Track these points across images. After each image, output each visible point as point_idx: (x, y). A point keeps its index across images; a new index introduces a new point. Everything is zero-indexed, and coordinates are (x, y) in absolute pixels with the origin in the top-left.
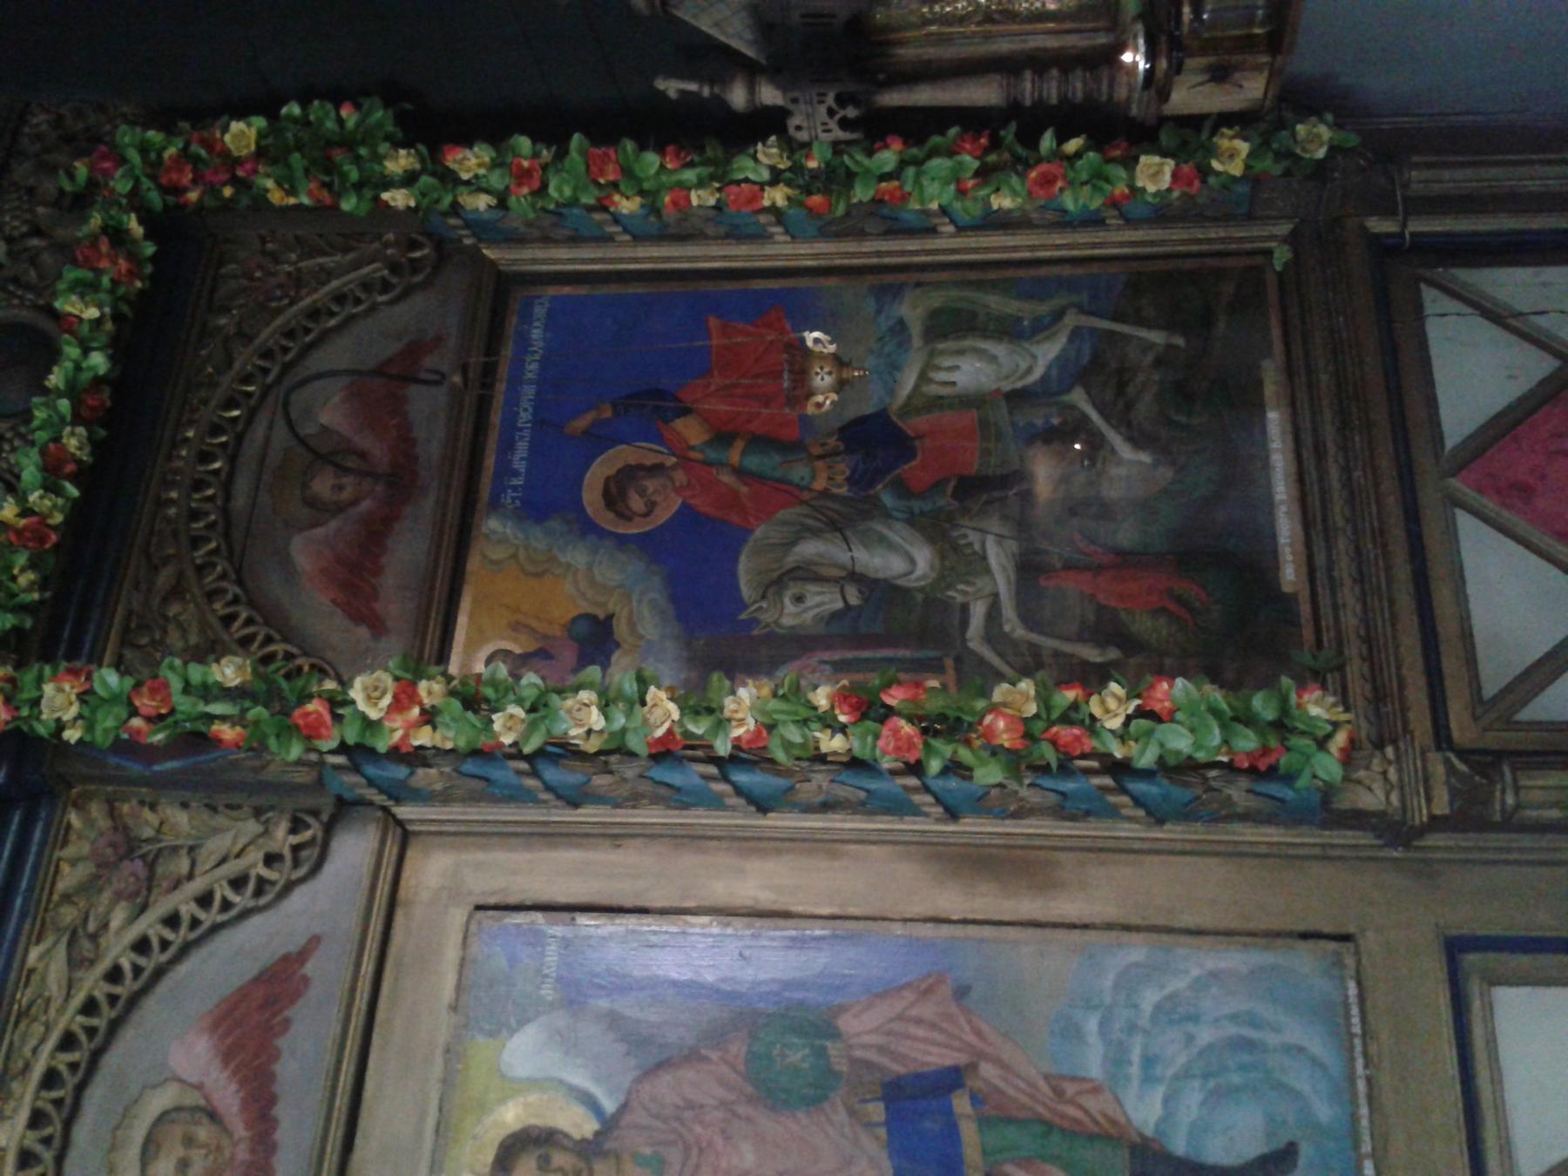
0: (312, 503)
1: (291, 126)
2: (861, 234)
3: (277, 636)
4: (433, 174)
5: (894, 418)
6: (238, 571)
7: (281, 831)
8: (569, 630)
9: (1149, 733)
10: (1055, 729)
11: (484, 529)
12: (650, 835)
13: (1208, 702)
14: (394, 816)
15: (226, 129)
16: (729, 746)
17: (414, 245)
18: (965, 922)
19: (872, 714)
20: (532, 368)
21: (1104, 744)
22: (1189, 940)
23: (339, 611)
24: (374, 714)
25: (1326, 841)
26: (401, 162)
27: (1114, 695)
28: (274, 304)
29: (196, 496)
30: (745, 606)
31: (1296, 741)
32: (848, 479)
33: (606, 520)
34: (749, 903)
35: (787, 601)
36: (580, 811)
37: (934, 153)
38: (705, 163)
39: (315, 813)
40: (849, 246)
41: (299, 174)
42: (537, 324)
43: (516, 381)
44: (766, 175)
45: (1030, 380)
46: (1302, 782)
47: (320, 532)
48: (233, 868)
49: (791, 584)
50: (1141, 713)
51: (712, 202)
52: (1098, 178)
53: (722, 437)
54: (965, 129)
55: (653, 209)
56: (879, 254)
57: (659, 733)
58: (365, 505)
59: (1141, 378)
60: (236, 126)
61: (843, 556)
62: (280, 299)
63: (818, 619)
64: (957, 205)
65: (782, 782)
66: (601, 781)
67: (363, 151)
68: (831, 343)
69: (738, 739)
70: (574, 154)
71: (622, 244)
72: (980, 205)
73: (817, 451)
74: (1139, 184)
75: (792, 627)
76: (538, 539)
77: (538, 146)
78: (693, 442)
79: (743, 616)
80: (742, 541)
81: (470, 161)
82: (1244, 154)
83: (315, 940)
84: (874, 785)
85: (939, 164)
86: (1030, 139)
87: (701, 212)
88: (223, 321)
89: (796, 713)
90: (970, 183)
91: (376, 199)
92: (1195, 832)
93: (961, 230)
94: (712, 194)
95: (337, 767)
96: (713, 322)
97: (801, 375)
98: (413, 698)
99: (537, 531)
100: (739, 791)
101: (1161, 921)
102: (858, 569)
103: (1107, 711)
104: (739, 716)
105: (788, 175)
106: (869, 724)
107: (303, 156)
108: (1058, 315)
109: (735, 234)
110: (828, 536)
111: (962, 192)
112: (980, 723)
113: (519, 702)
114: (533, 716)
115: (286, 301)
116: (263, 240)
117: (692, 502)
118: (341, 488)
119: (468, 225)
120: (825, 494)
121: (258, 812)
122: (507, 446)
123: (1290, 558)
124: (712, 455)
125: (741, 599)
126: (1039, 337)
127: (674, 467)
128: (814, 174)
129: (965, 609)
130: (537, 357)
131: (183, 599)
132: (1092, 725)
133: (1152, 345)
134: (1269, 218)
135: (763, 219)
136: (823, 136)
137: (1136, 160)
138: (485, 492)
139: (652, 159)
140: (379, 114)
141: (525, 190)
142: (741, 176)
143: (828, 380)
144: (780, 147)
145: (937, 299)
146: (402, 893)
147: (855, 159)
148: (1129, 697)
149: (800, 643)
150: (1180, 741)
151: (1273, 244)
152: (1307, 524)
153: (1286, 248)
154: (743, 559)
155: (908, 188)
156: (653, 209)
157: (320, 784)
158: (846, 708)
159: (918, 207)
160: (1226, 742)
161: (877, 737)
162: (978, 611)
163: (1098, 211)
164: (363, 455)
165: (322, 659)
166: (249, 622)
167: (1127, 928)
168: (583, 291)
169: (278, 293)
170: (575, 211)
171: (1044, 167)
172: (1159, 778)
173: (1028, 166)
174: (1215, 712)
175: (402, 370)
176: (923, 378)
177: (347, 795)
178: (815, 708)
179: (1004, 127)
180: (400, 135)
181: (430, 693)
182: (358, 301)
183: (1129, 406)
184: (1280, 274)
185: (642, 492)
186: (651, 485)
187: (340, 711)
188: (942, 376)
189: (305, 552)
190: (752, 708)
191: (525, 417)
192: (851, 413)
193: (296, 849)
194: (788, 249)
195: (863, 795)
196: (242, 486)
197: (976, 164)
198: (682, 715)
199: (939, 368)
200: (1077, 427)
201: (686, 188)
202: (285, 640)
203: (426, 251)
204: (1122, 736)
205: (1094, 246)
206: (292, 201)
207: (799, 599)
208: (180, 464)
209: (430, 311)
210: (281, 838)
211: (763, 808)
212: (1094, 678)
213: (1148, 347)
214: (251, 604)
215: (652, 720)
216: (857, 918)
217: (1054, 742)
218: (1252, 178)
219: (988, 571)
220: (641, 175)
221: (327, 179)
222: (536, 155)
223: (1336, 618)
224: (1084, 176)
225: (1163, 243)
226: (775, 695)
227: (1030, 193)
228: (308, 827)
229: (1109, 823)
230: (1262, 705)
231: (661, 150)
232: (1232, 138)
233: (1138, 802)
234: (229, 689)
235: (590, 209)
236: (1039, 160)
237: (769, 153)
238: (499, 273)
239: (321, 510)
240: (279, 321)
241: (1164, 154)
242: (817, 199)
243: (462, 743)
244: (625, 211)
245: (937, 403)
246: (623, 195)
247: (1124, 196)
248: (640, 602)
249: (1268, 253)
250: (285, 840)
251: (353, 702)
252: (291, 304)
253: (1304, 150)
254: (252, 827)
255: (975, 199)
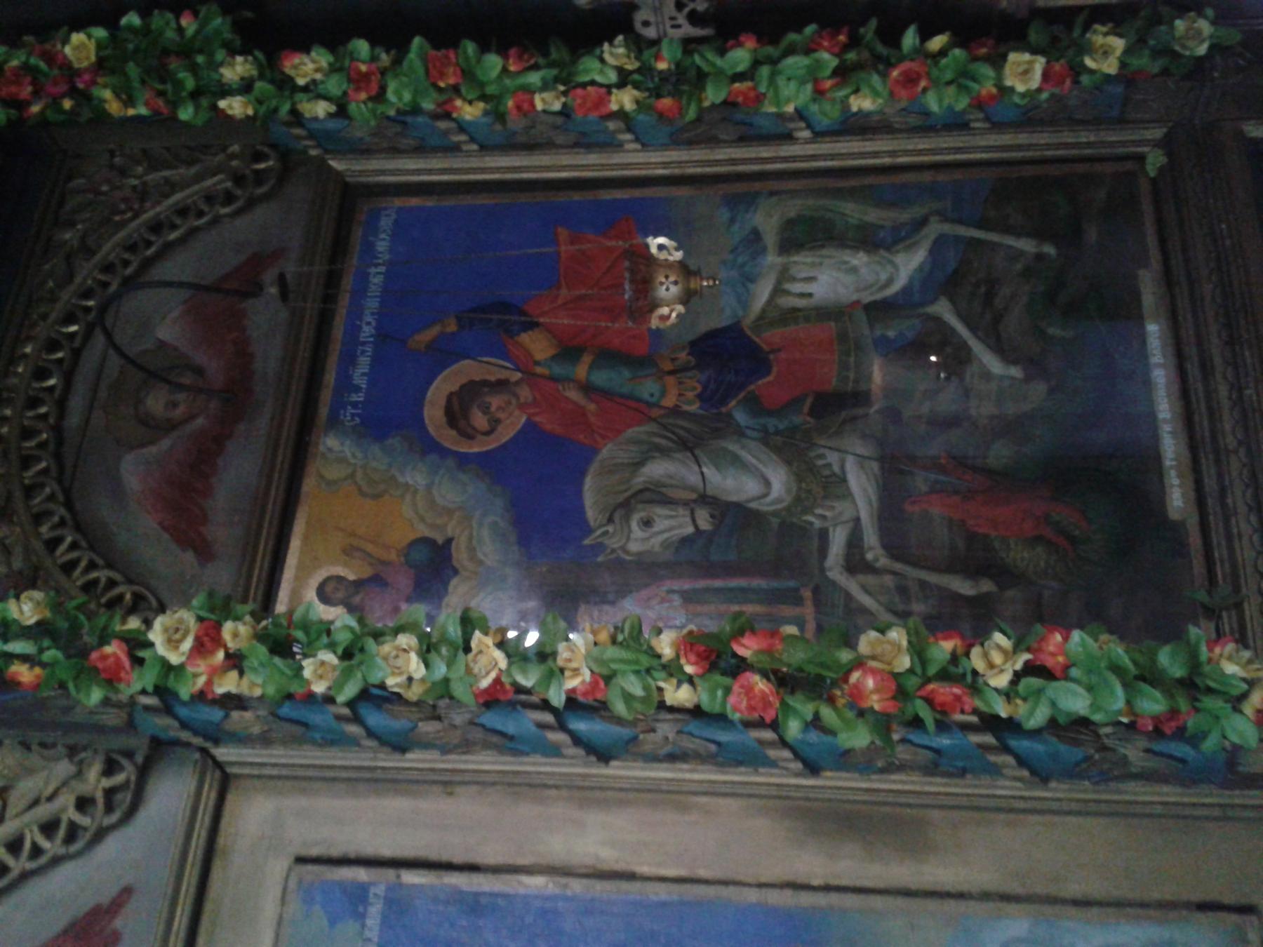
0: (146, 421)
1: (131, 37)
2: (712, 141)
3: (100, 562)
4: (272, 82)
5: (749, 333)
6: (67, 492)
7: (93, 773)
8: (406, 556)
9: (1039, 692)
10: (931, 686)
11: (322, 448)
12: (481, 782)
13: (1109, 658)
14: (213, 758)
15: (66, 41)
16: (563, 698)
17: (259, 157)
18: (827, 888)
19: (722, 664)
20: (376, 280)
21: (987, 703)
22: (1073, 911)
23: (166, 536)
24: (175, 659)
25: (1227, 801)
26: (236, 69)
27: (999, 647)
28: (117, 218)
29: (30, 414)
30: (590, 531)
31: (1208, 702)
32: (699, 396)
33: (448, 438)
34: (589, 861)
35: (634, 525)
36: (409, 756)
37: (791, 51)
38: (551, 65)
39: (129, 755)
40: (698, 154)
41: (136, 84)
42: (383, 236)
43: (360, 292)
44: (613, 77)
45: (889, 292)
46: (1209, 745)
47: (153, 449)
48: (44, 812)
49: (640, 506)
50: (1030, 669)
51: (557, 106)
52: (963, 77)
53: (569, 351)
54: (823, 26)
55: (499, 116)
56: (733, 162)
57: (485, 683)
58: (200, 421)
59: (1005, 291)
60: (77, 38)
61: (693, 479)
62: (123, 212)
63: (666, 545)
64: (814, 108)
65: (626, 732)
66: (428, 728)
67: (200, 59)
68: (677, 249)
69: (573, 690)
70: (413, 55)
71: (469, 154)
72: (838, 107)
73: (668, 366)
74: (1008, 83)
75: (639, 554)
76: (377, 458)
77: (378, 50)
78: (539, 356)
79: (587, 542)
80: (588, 460)
81: (307, 66)
82: (1118, 52)
83: (127, 892)
84: (724, 737)
85: (796, 63)
86: (891, 37)
87: (550, 119)
88: (68, 236)
89: (637, 662)
90: (828, 84)
91: (214, 107)
92: (1085, 791)
93: (819, 135)
94: (558, 98)
95: (147, 708)
96: (563, 233)
97: (644, 285)
98: (218, 642)
99: (376, 449)
100: (577, 740)
101: (1040, 889)
102: (709, 492)
103: (991, 666)
104: (574, 665)
105: (636, 77)
106: (718, 678)
107: (138, 65)
108: (923, 222)
109: (584, 143)
110: (678, 455)
111: (819, 93)
112: (846, 680)
113: (332, 646)
114: (346, 663)
115: (129, 215)
116: (112, 154)
117: (537, 419)
118: (175, 405)
119: (312, 135)
120: (676, 411)
121: (72, 751)
122: (349, 359)
123: (1176, 481)
124: (558, 370)
125: (586, 522)
126: (900, 246)
127: (517, 383)
128: (664, 77)
129: (824, 535)
130: (382, 269)
131: (11, 521)
132: (974, 683)
133: (1022, 253)
134: (1142, 121)
135: (611, 125)
136: (671, 32)
137: (1004, 58)
138: (324, 411)
139: (493, 62)
140: (218, 21)
141: (363, 96)
142: (587, 79)
143: (674, 290)
144: (627, 46)
145: (794, 207)
146: (221, 841)
147: (707, 59)
148: (1017, 649)
149: (647, 570)
150: (1075, 701)
151: (1146, 149)
152: (1193, 446)
153: (1160, 152)
154: (589, 482)
155: (762, 89)
156: (499, 116)
157: (131, 725)
158: (693, 658)
159: (773, 110)
160: (1128, 702)
161: (728, 691)
162: (838, 539)
163: (964, 112)
164: (199, 371)
165: (148, 588)
166: (74, 546)
167: (1006, 898)
168: (430, 202)
169: (123, 206)
170: (420, 119)
171: (906, 65)
172: (1046, 736)
173: (890, 65)
174: (1116, 669)
175: (243, 283)
176: (778, 291)
177: (162, 735)
178: (659, 657)
179: (864, 23)
180: (238, 43)
181: (235, 635)
182: (201, 214)
183: (998, 319)
184: (1154, 181)
185: (486, 410)
186: (495, 401)
187: (141, 654)
188: (797, 288)
189: (134, 472)
190: (588, 656)
191: (367, 331)
192: (704, 326)
193: (110, 793)
194: (641, 158)
195: (713, 748)
196: (76, 403)
197: (834, 62)
198: (510, 664)
199: (794, 279)
200: (943, 339)
201: (529, 91)
202: (110, 566)
203: (271, 163)
204: (1008, 694)
205: (958, 150)
206: (131, 112)
207: (647, 523)
208: (15, 381)
209: (277, 224)
210: (94, 781)
211: (603, 755)
212: (975, 620)
213: (1017, 255)
214: (78, 528)
215: (476, 670)
216: (706, 882)
217: (929, 701)
218: (1127, 77)
219: (848, 495)
220: (485, 79)
221: (160, 87)
222: (374, 59)
223: (1231, 549)
224: (949, 76)
225: (1029, 147)
226: (614, 641)
227: (892, 94)
228: (122, 769)
229: (986, 780)
230: (1169, 660)
231: (503, 52)
232: (1106, 34)
233: (1022, 762)
234: (29, 627)
235: (436, 116)
236: (902, 59)
237: (616, 53)
238: (346, 184)
239: (156, 428)
240: (121, 235)
241: (1035, 51)
242: (667, 102)
243: (271, 690)
244: (468, 117)
245: (791, 315)
246: (464, 99)
247: (992, 98)
248: (481, 525)
249: (1141, 158)
250: (99, 781)
251: (151, 645)
252: (136, 216)
253: (1184, 47)
254: (64, 768)
255: (833, 100)
